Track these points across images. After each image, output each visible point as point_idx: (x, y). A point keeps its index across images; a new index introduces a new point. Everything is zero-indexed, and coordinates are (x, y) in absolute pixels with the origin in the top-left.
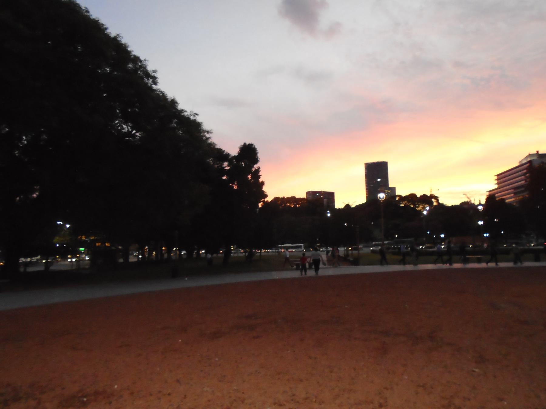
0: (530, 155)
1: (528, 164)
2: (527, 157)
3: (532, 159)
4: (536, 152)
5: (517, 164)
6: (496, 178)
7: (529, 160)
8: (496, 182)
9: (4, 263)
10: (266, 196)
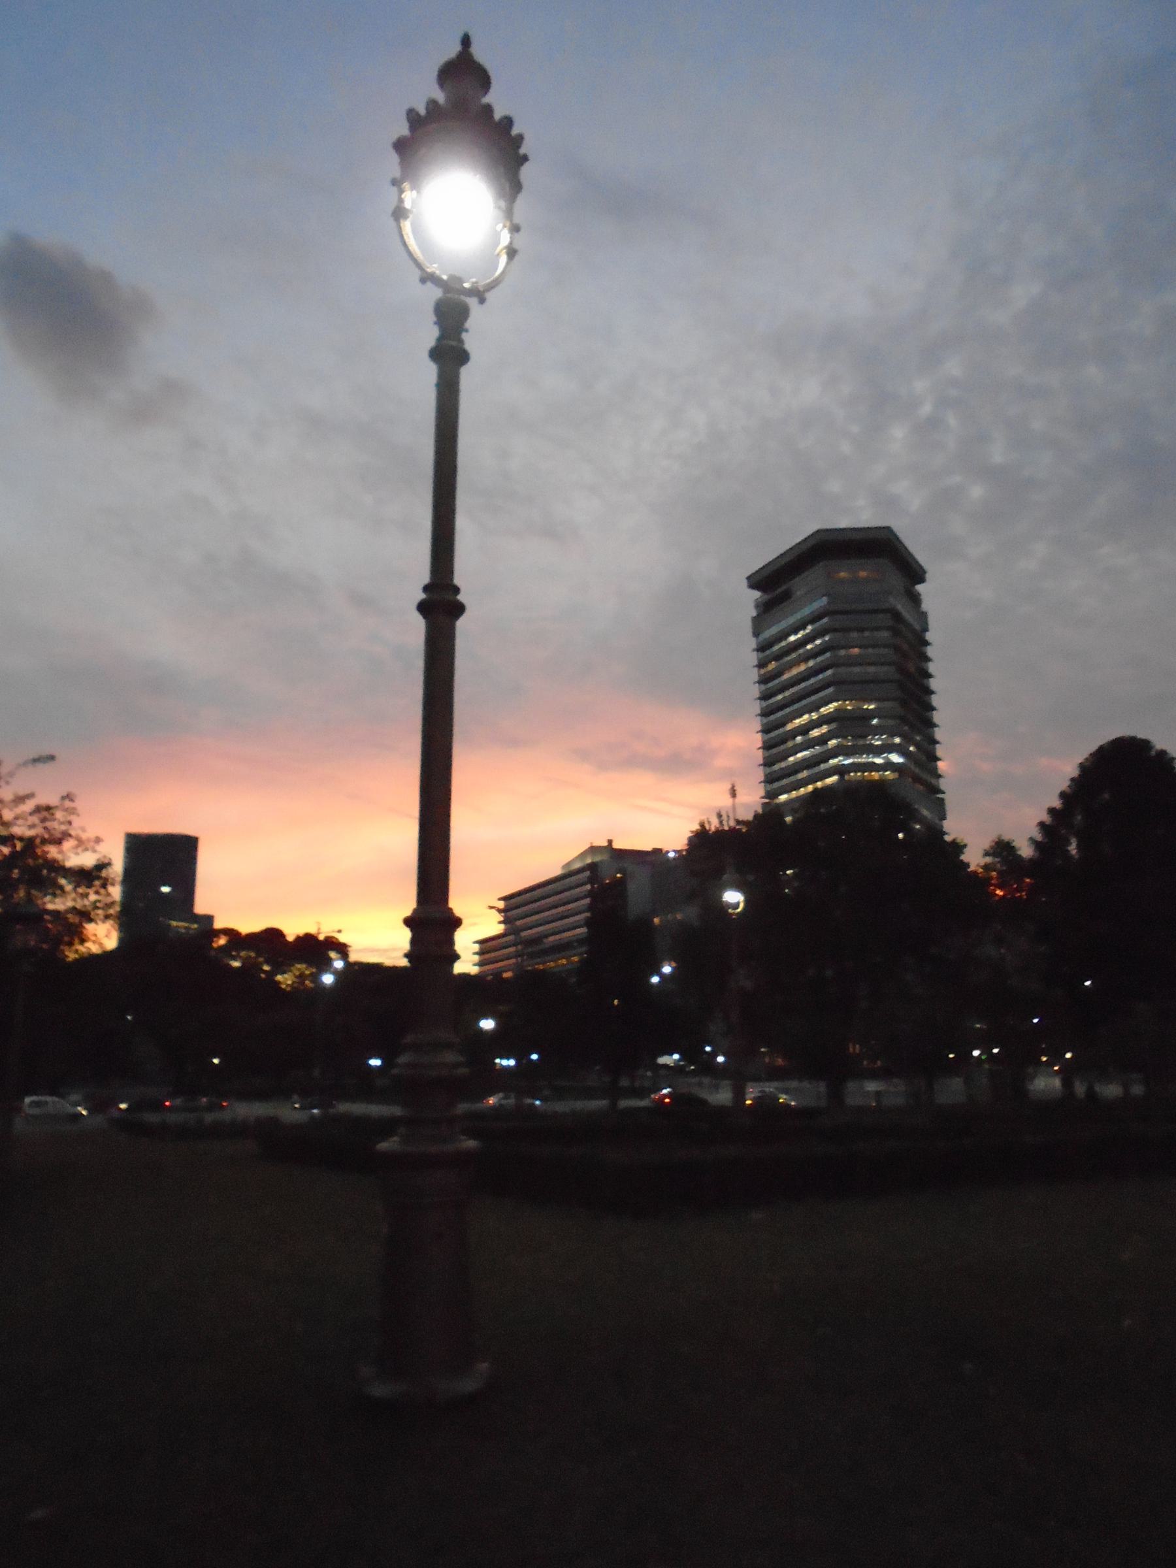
0: (593, 850)
1: (588, 873)
2: (583, 855)
3: (597, 859)
4: (605, 844)
5: (557, 871)
6: (477, 947)
7: (589, 861)
8: (476, 958)
9: (674, 969)
10: (83, 941)
